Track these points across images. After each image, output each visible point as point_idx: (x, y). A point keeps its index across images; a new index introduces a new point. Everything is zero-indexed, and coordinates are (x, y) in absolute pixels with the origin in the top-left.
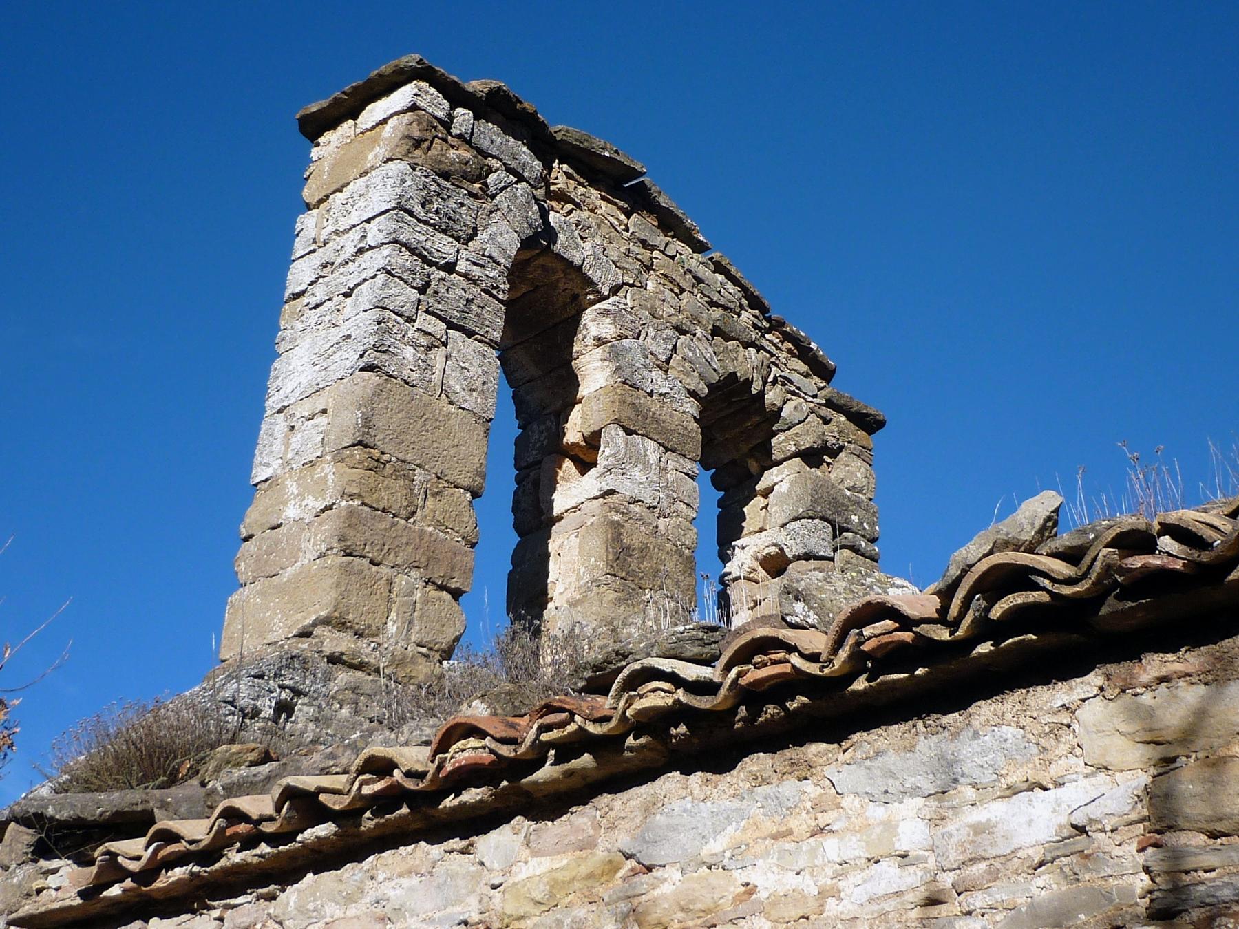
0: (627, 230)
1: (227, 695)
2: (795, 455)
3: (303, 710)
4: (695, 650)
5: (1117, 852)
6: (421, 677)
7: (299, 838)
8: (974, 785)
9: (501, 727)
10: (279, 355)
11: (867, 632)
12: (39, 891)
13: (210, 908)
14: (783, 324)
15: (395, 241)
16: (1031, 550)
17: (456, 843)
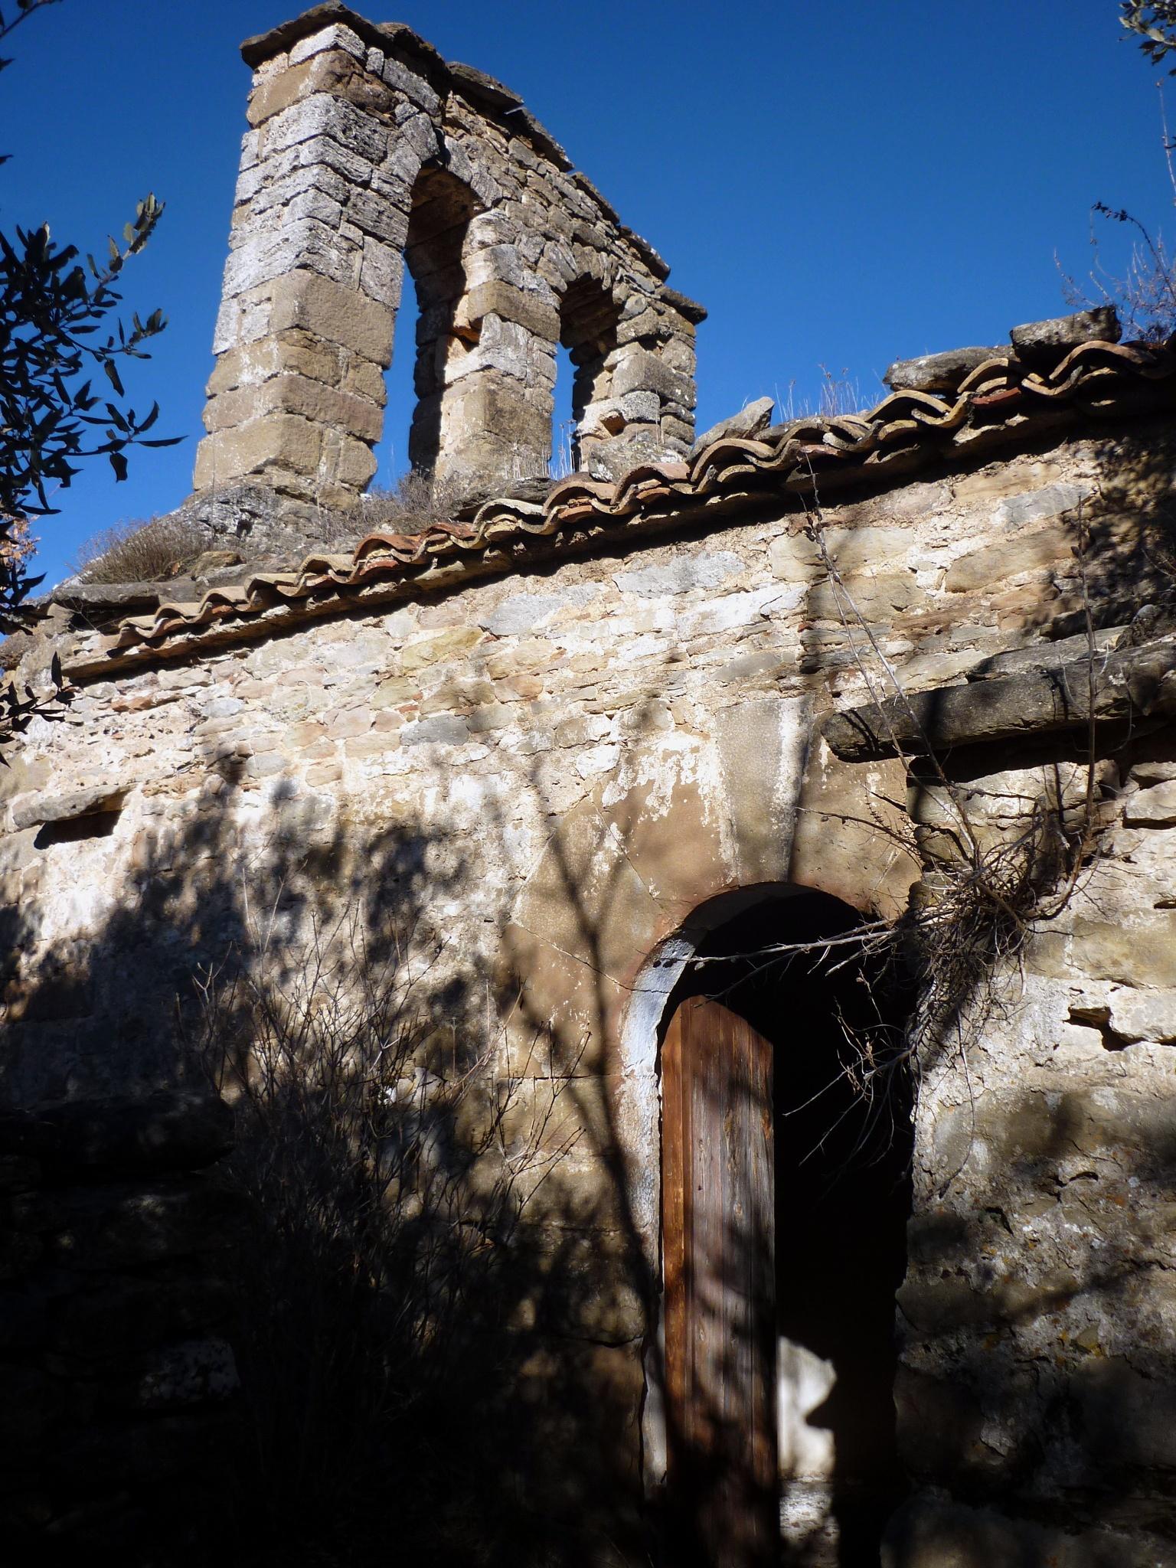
0: (507, 152)
1: (203, 516)
2: (634, 340)
3: (258, 527)
4: (531, 494)
5: (787, 631)
6: (345, 505)
7: (264, 615)
8: (705, 588)
9: (401, 542)
10: (232, 251)
11: (641, 486)
12: (76, 652)
13: (200, 663)
14: (630, 233)
15: (322, 162)
16: (750, 437)
17: (371, 620)
